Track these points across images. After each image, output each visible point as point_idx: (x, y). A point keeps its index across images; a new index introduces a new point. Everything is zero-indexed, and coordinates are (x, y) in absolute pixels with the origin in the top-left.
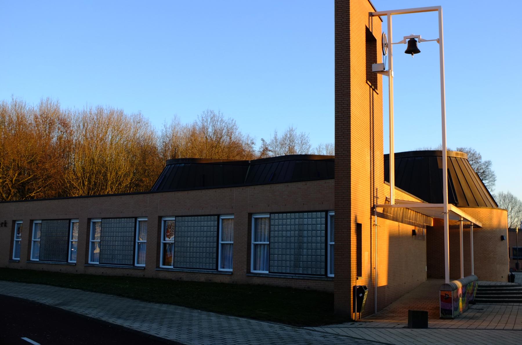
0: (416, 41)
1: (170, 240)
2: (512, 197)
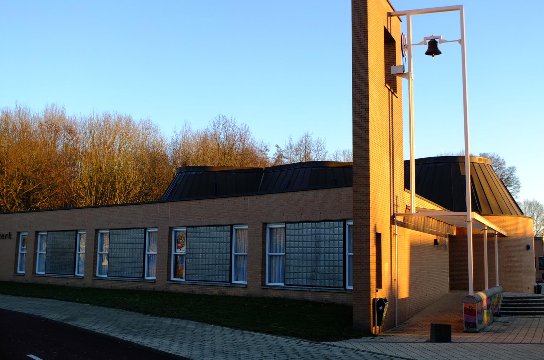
0: (437, 42)
1: (182, 251)
2: (538, 204)
